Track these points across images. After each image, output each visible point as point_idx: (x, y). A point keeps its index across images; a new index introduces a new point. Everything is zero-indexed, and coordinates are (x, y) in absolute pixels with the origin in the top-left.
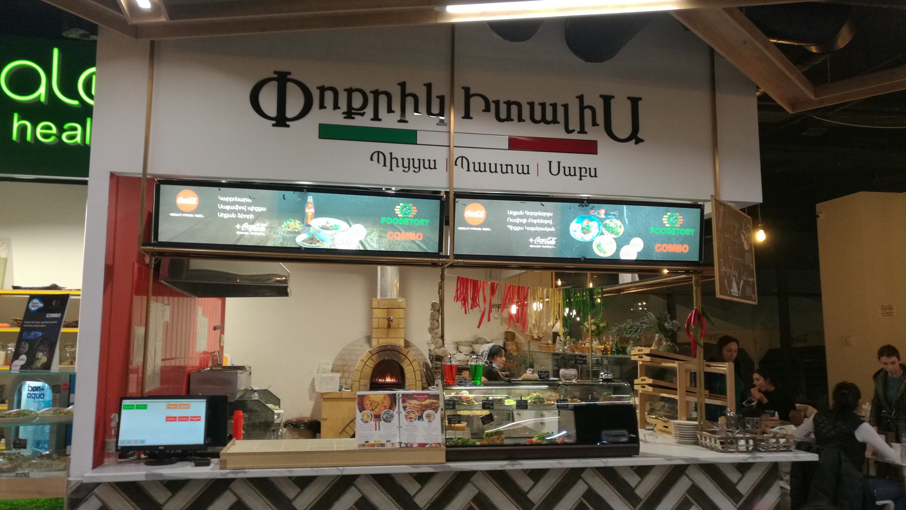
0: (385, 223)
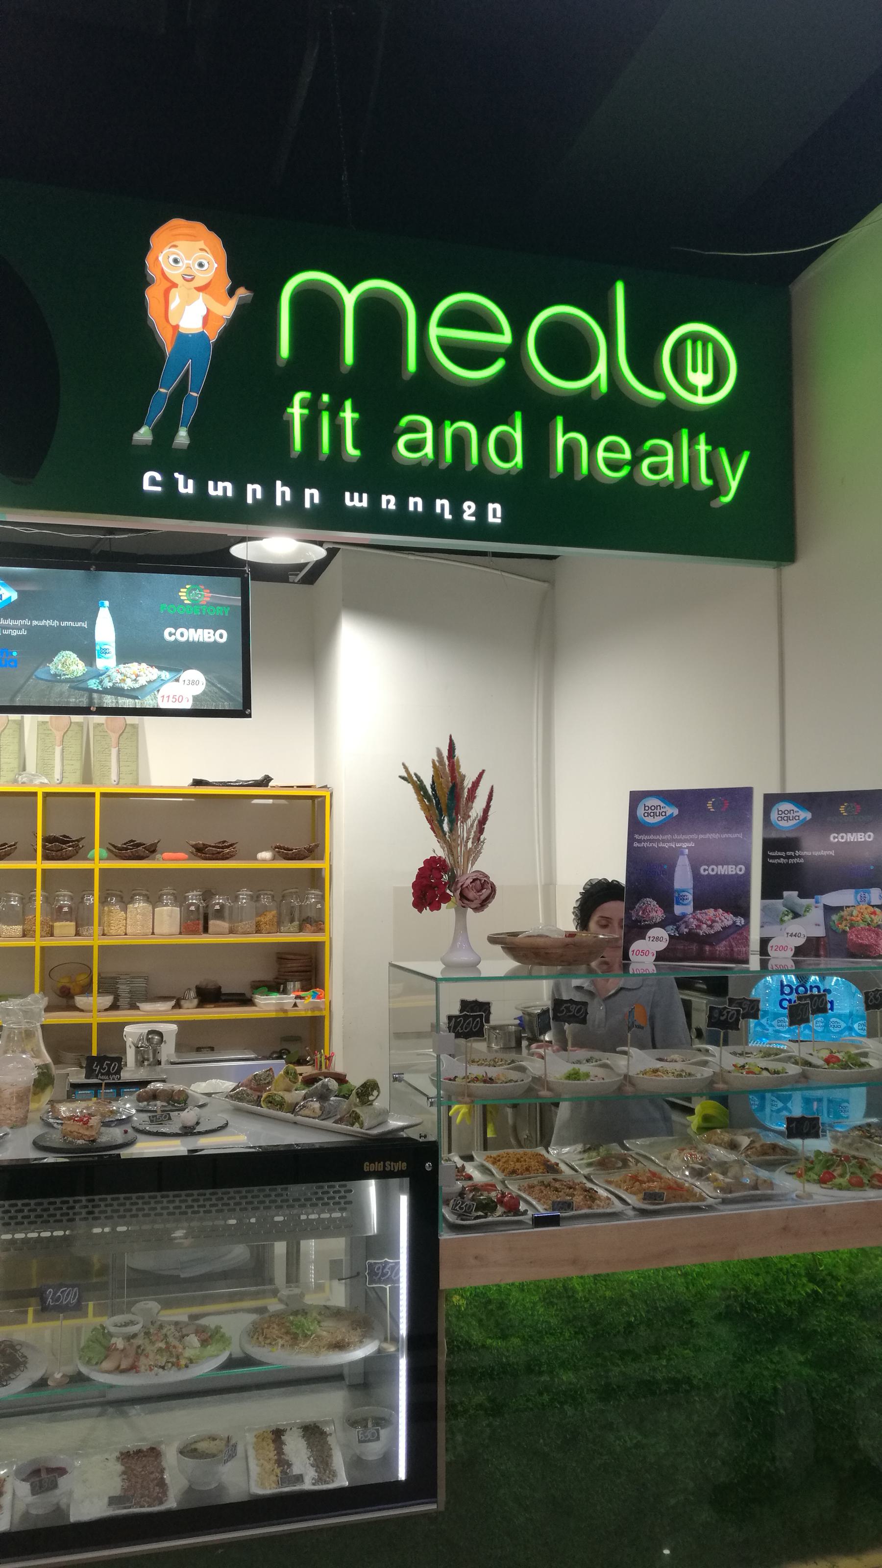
0: (166, 612)
